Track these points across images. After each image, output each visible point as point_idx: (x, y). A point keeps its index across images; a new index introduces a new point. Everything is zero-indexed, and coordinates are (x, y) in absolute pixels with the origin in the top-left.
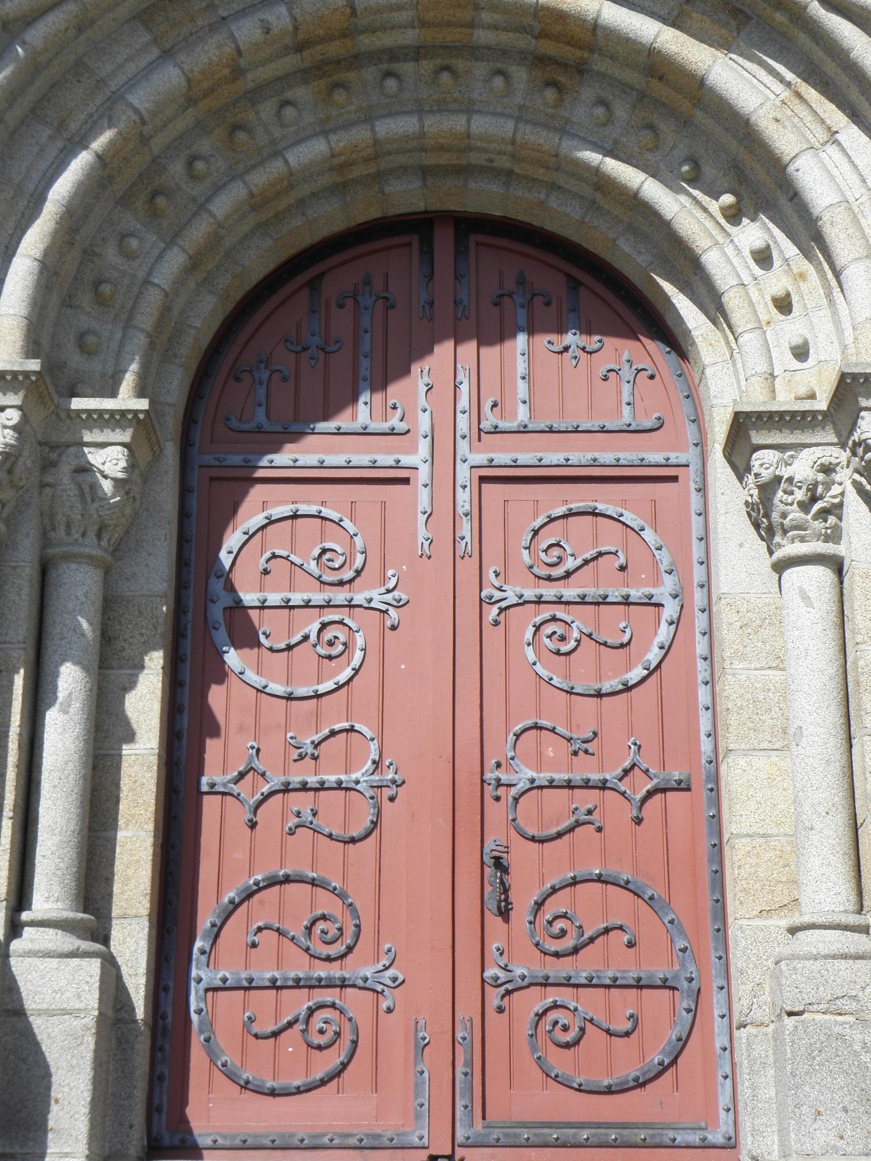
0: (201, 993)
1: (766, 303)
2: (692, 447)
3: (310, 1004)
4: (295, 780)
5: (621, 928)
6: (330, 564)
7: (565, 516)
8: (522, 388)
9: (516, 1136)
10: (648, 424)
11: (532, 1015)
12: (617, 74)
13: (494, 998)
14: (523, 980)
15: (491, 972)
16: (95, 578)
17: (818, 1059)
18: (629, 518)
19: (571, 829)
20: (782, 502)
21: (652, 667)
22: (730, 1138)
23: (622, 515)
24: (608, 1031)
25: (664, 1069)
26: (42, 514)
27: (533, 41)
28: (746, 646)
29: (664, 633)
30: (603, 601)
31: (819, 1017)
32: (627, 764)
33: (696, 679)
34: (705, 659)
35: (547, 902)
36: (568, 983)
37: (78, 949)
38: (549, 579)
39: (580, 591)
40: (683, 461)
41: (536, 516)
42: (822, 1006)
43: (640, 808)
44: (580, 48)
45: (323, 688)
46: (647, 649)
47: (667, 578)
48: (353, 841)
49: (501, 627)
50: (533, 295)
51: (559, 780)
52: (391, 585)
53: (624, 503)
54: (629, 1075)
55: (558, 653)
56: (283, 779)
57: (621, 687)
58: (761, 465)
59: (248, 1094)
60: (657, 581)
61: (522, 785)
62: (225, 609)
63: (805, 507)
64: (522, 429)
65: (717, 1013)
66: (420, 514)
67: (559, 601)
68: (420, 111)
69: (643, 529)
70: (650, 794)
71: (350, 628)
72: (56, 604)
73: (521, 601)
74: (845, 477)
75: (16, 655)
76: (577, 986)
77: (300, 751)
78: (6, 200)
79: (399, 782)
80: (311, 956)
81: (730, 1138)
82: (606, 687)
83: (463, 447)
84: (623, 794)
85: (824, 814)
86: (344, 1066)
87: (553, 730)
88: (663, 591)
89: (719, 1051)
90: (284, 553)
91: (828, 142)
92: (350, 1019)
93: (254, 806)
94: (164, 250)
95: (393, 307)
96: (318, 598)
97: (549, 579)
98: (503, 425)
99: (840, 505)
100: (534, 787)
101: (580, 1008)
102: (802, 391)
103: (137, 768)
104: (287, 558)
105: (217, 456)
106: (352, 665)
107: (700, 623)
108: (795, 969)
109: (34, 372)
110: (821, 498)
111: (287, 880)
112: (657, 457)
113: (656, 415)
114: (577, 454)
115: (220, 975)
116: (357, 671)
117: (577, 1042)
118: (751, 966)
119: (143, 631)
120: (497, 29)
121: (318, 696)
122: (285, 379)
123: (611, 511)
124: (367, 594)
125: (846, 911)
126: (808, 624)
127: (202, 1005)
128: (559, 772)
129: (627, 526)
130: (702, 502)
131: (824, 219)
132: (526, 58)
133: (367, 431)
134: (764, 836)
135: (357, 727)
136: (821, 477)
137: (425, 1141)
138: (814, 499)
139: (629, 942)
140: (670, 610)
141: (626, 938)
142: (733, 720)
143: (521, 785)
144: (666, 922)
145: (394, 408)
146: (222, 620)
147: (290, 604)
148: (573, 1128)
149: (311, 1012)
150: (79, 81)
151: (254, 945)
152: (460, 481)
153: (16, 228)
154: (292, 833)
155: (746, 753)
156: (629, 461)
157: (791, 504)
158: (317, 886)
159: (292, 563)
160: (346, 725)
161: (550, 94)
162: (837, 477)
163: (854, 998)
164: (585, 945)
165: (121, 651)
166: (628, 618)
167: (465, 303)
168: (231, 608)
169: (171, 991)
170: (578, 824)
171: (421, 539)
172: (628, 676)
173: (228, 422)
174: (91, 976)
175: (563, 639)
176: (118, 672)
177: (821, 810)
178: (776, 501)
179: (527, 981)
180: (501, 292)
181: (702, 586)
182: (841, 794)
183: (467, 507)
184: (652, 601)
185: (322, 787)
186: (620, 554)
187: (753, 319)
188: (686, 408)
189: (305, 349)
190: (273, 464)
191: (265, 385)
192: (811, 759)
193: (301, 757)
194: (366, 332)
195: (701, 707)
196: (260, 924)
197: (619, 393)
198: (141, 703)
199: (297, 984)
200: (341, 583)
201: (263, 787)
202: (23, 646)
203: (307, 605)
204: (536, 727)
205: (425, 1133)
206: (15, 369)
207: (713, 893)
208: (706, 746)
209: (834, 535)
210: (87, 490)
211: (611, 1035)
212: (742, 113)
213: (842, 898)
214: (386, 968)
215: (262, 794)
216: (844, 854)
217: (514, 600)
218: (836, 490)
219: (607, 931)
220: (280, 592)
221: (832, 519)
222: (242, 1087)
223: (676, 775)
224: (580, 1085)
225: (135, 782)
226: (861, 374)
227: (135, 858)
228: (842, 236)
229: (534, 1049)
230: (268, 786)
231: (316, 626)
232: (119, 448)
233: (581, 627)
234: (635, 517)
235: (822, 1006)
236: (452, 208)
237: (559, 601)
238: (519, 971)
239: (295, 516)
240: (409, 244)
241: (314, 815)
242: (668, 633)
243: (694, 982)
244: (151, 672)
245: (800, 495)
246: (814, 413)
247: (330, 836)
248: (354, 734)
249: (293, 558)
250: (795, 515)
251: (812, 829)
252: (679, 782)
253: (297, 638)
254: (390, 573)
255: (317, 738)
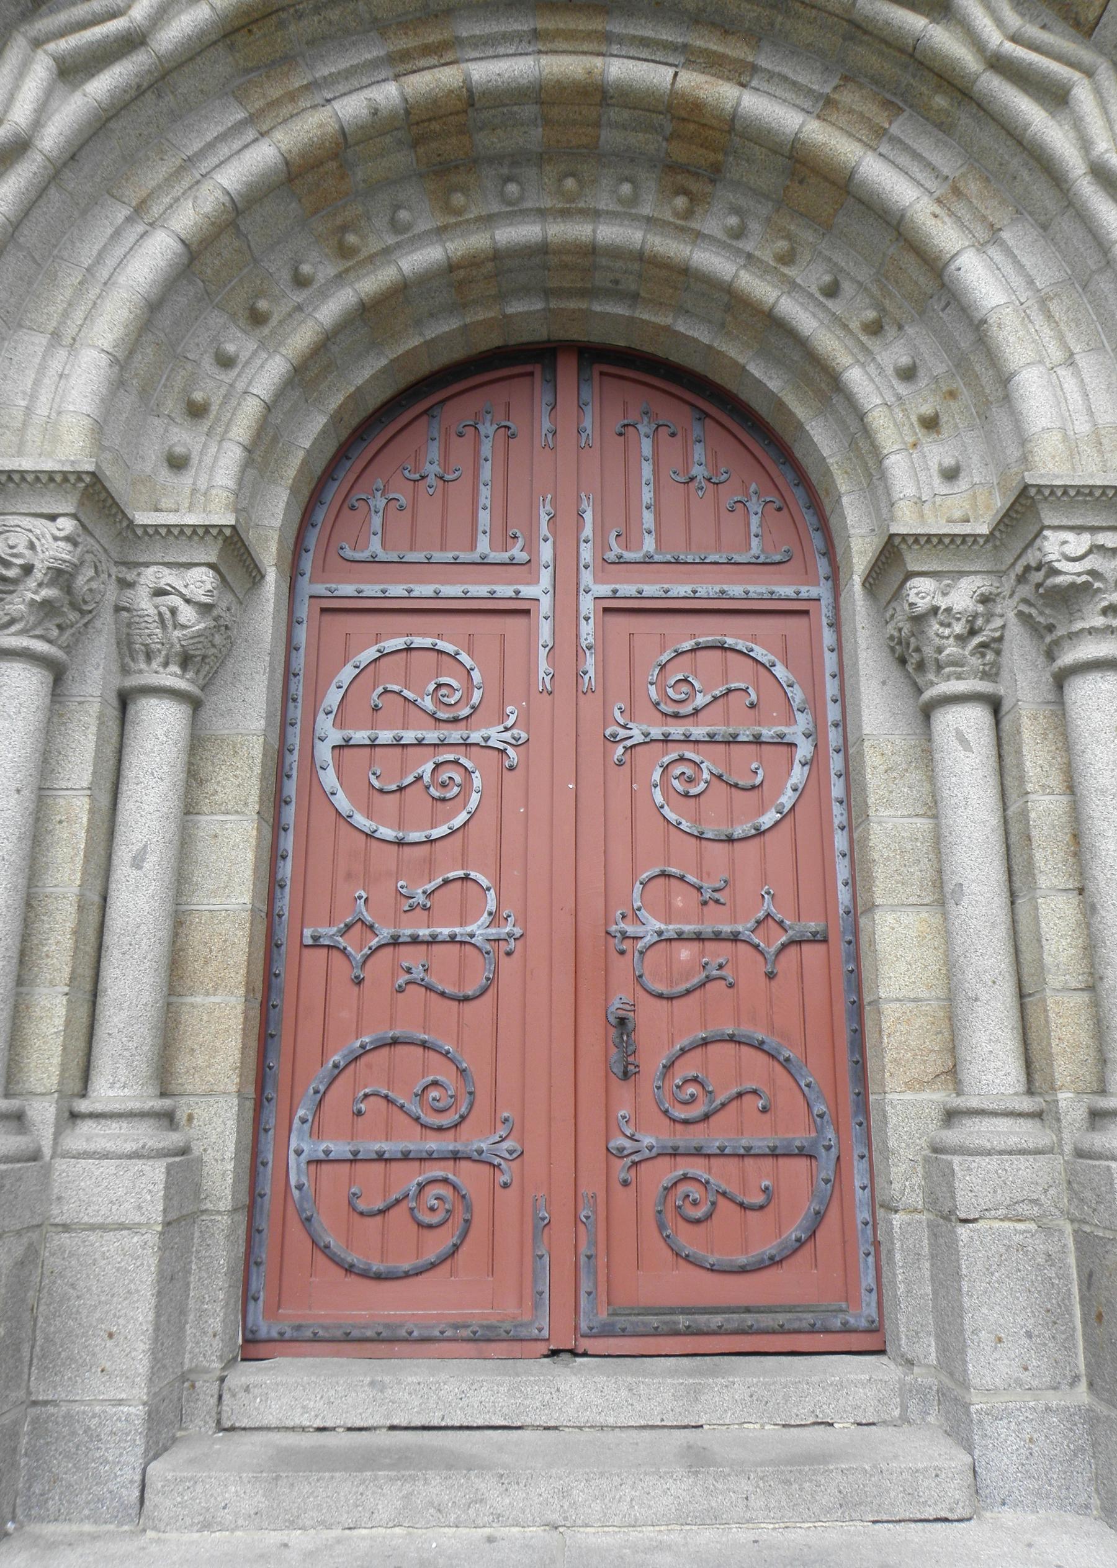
0: (303, 1166)
1: (912, 424)
2: (822, 581)
3: (420, 1179)
4: (406, 932)
5: (755, 1092)
6: (445, 700)
7: (692, 650)
8: (648, 519)
9: (645, 1324)
10: (777, 558)
11: (661, 1189)
12: (752, 182)
13: (620, 1168)
14: (650, 1150)
15: (620, 1141)
16: (179, 716)
17: (996, 1274)
18: (759, 653)
19: (703, 985)
20: (938, 635)
21: (786, 810)
22: (873, 1322)
23: (752, 650)
24: (741, 1205)
25: (800, 1243)
26: (118, 643)
27: (664, 144)
28: (891, 792)
29: (798, 775)
30: (732, 741)
31: (996, 1224)
32: (761, 914)
33: (832, 823)
34: (841, 802)
35: (677, 1064)
36: (698, 1153)
37: (143, 1147)
38: (676, 716)
39: (708, 729)
40: (815, 596)
41: (663, 650)
42: (999, 1212)
43: (774, 962)
44: (714, 150)
45: (436, 833)
46: (781, 792)
47: (798, 715)
48: (466, 999)
49: (627, 767)
50: (659, 426)
51: (689, 933)
52: (509, 723)
53: (754, 639)
54: (764, 1253)
55: (686, 795)
56: (392, 931)
57: (753, 832)
58: (917, 594)
59: (351, 1279)
60: (791, 720)
61: (650, 939)
62: (334, 747)
63: (961, 639)
64: (647, 560)
65: (857, 1184)
66: (541, 648)
67: (687, 740)
68: (542, 214)
69: (774, 665)
70: (784, 946)
71: (466, 768)
72: (133, 744)
73: (647, 740)
74: (1007, 610)
75: (79, 803)
76: (709, 1156)
77: (411, 901)
78: (73, 285)
79: (518, 935)
80: (422, 1125)
81: (873, 1322)
82: (738, 832)
83: (587, 577)
84: (756, 947)
85: (990, 983)
86: (456, 1247)
87: (682, 878)
88: (797, 730)
89: (860, 1226)
90: (396, 688)
91: (988, 242)
92: (464, 1197)
93: (362, 960)
94: (267, 360)
95: (513, 436)
96: (432, 736)
97: (676, 716)
98: (629, 556)
99: (1000, 639)
100: (663, 940)
101: (712, 1181)
102: (957, 514)
103: (227, 925)
104: (399, 693)
105: (328, 586)
106: (468, 808)
107: (836, 763)
108: (969, 1169)
109: (87, 473)
110: (981, 630)
111: (395, 1042)
112: (787, 591)
113: (785, 548)
114: (705, 586)
115: (323, 1146)
116: (472, 815)
117: (709, 1216)
118: (903, 1145)
119: (238, 772)
120: (626, 129)
121: (431, 841)
122: (401, 508)
123: (741, 645)
124: (484, 732)
125: (1016, 1094)
126: (967, 769)
127: (304, 1180)
128: (689, 923)
129: (757, 661)
130: (835, 637)
131: (990, 321)
132: (655, 166)
133: (485, 561)
134: (915, 1000)
135: (473, 875)
136: (980, 608)
137: (545, 1333)
138: (973, 632)
139: (764, 1107)
140: (804, 750)
141: (760, 1104)
142: (880, 873)
143: (648, 938)
144: (803, 1084)
145: (515, 537)
146: (331, 762)
147: (402, 742)
148: (705, 1313)
149: (421, 1187)
150: (162, 159)
151: (359, 1113)
152: (584, 612)
153: (85, 319)
154: (401, 990)
155: (893, 908)
156: (759, 594)
157: (948, 638)
158: (429, 1048)
159: (405, 698)
160: (460, 873)
161: (681, 202)
162: (998, 610)
163: (1035, 1202)
164: (716, 1111)
165: (212, 795)
166: (760, 759)
167: (589, 431)
168: (340, 747)
169: (270, 1165)
170: (709, 979)
171: (541, 674)
172: (761, 820)
173: (341, 552)
174: (154, 1184)
175: (690, 780)
176: (209, 818)
177: (987, 978)
178: (931, 633)
179: (655, 1152)
180: (626, 422)
181: (836, 725)
182: (1007, 960)
183: (591, 640)
184: (785, 741)
185: (433, 941)
186: (751, 690)
187: (899, 440)
188: (817, 540)
189: (423, 478)
190: (387, 594)
191: (381, 514)
192: (974, 921)
193: (412, 908)
194: (486, 460)
195: (837, 853)
196: (367, 1090)
197: (748, 525)
198: (233, 853)
199: (406, 1157)
200: (456, 720)
201: (371, 941)
202: (88, 792)
203: (420, 743)
204: (664, 875)
205: (545, 1324)
206: (65, 469)
207: (852, 1052)
208: (843, 895)
209: (991, 674)
210: (168, 615)
211: (745, 1208)
212: (895, 208)
213: (1011, 1079)
214: (503, 1140)
215: (370, 948)
216: (1013, 1028)
217: (641, 739)
218: (997, 623)
219: (740, 1095)
220: (392, 729)
221: (990, 656)
222: (346, 1270)
223: (813, 926)
224: (713, 1265)
225: (225, 941)
226: (1046, 486)
227: (223, 1027)
228: (1011, 339)
229: (661, 1227)
230: (377, 939)
231: (430, 766)
232: (204, 569)
233: (711, 767)
234: (765, 652)
235: (999, 1212)
236: (575, 337)
237: (687, 740)
238: (648, 1140)
239: (409, 649)
240: (531, 374)
241: (426, 970)
242: (802, 774)
243: (833, 1149)
244: (245, 818)
245: (959, 628)
246: (975, 537)
247: (443, 994)
248: (470, 884)
249: (406, 693)
250: (952, 649)
251: (976, 1000)
252: (814, 934)
253: (410, 779)
254: (509, 709)
255: (430, 887)
